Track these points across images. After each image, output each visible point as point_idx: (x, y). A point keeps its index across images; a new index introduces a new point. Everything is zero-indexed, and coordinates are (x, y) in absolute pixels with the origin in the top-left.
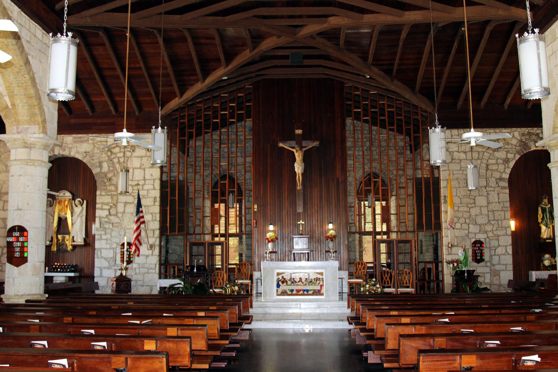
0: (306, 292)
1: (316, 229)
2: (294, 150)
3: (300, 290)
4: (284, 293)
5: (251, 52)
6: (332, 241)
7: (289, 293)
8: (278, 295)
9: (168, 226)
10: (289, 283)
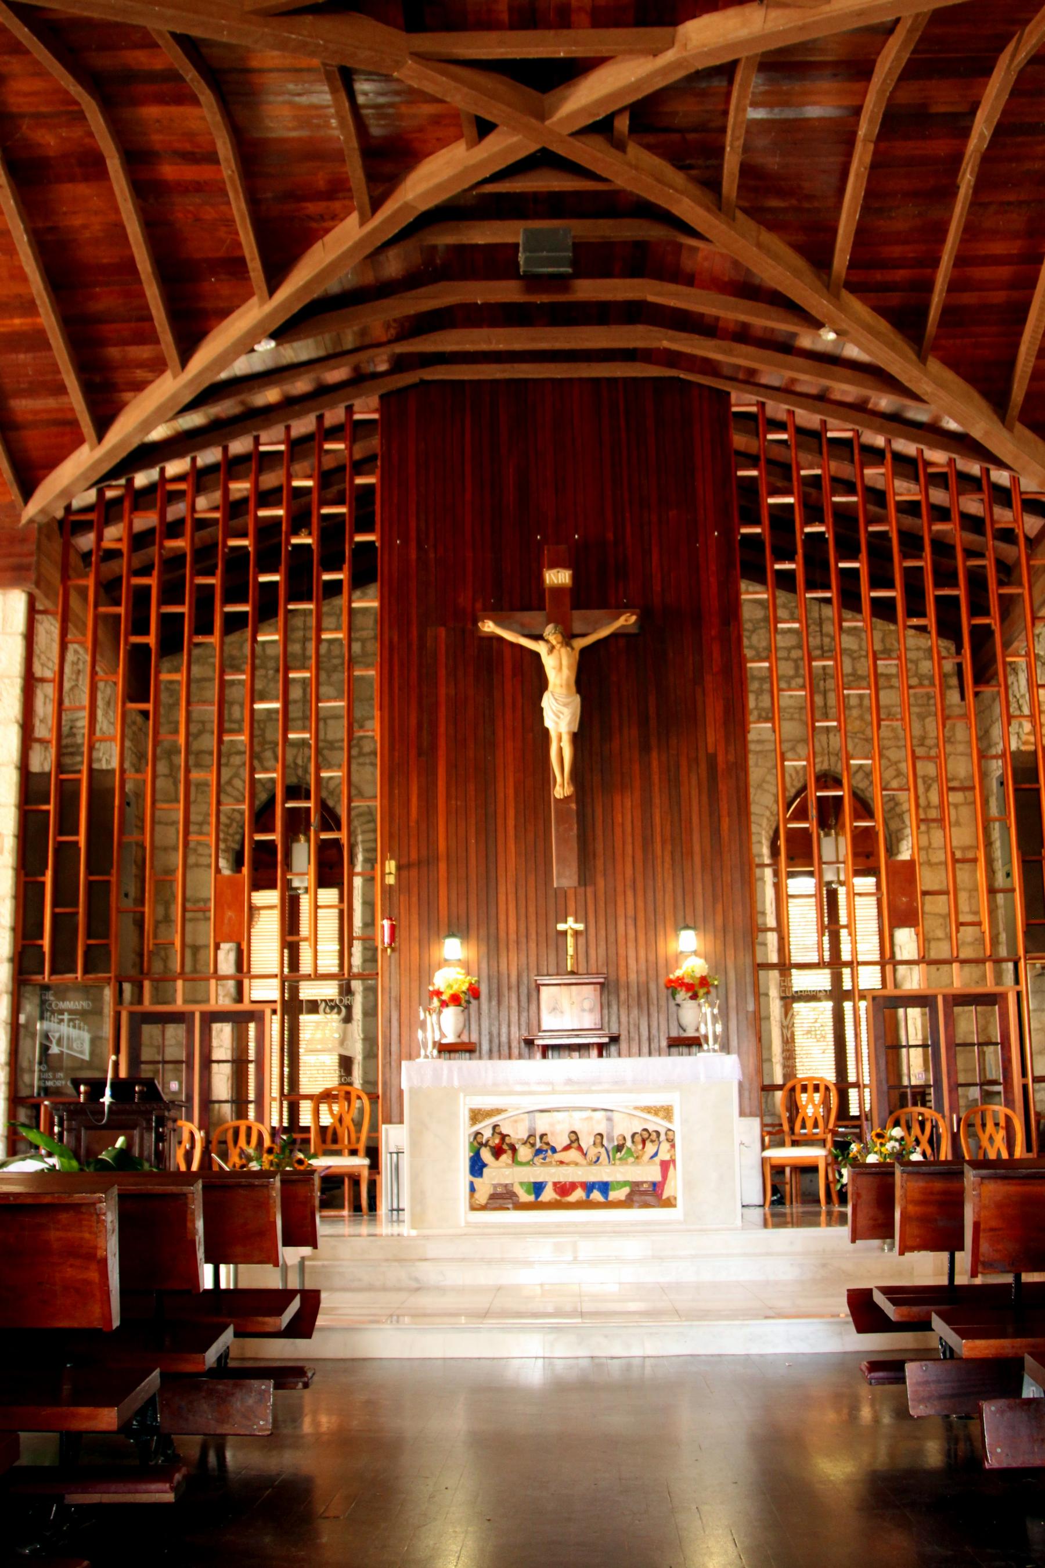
0: (597, 1194)
1: (632, 954)
2: (540, 648)
3: (573, 1186)
4: (503, 1199)
5: (363, 222)
6: (694, 997)
7: (526, 1197)
8: (473, 1208)
9: (47, 949)
10: (524, 1153)
